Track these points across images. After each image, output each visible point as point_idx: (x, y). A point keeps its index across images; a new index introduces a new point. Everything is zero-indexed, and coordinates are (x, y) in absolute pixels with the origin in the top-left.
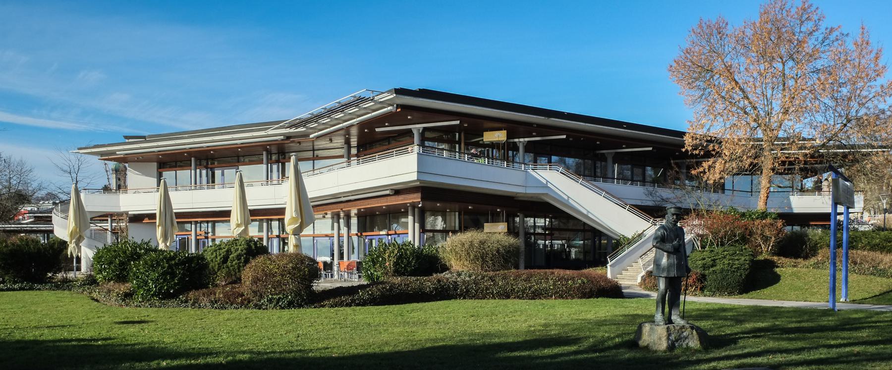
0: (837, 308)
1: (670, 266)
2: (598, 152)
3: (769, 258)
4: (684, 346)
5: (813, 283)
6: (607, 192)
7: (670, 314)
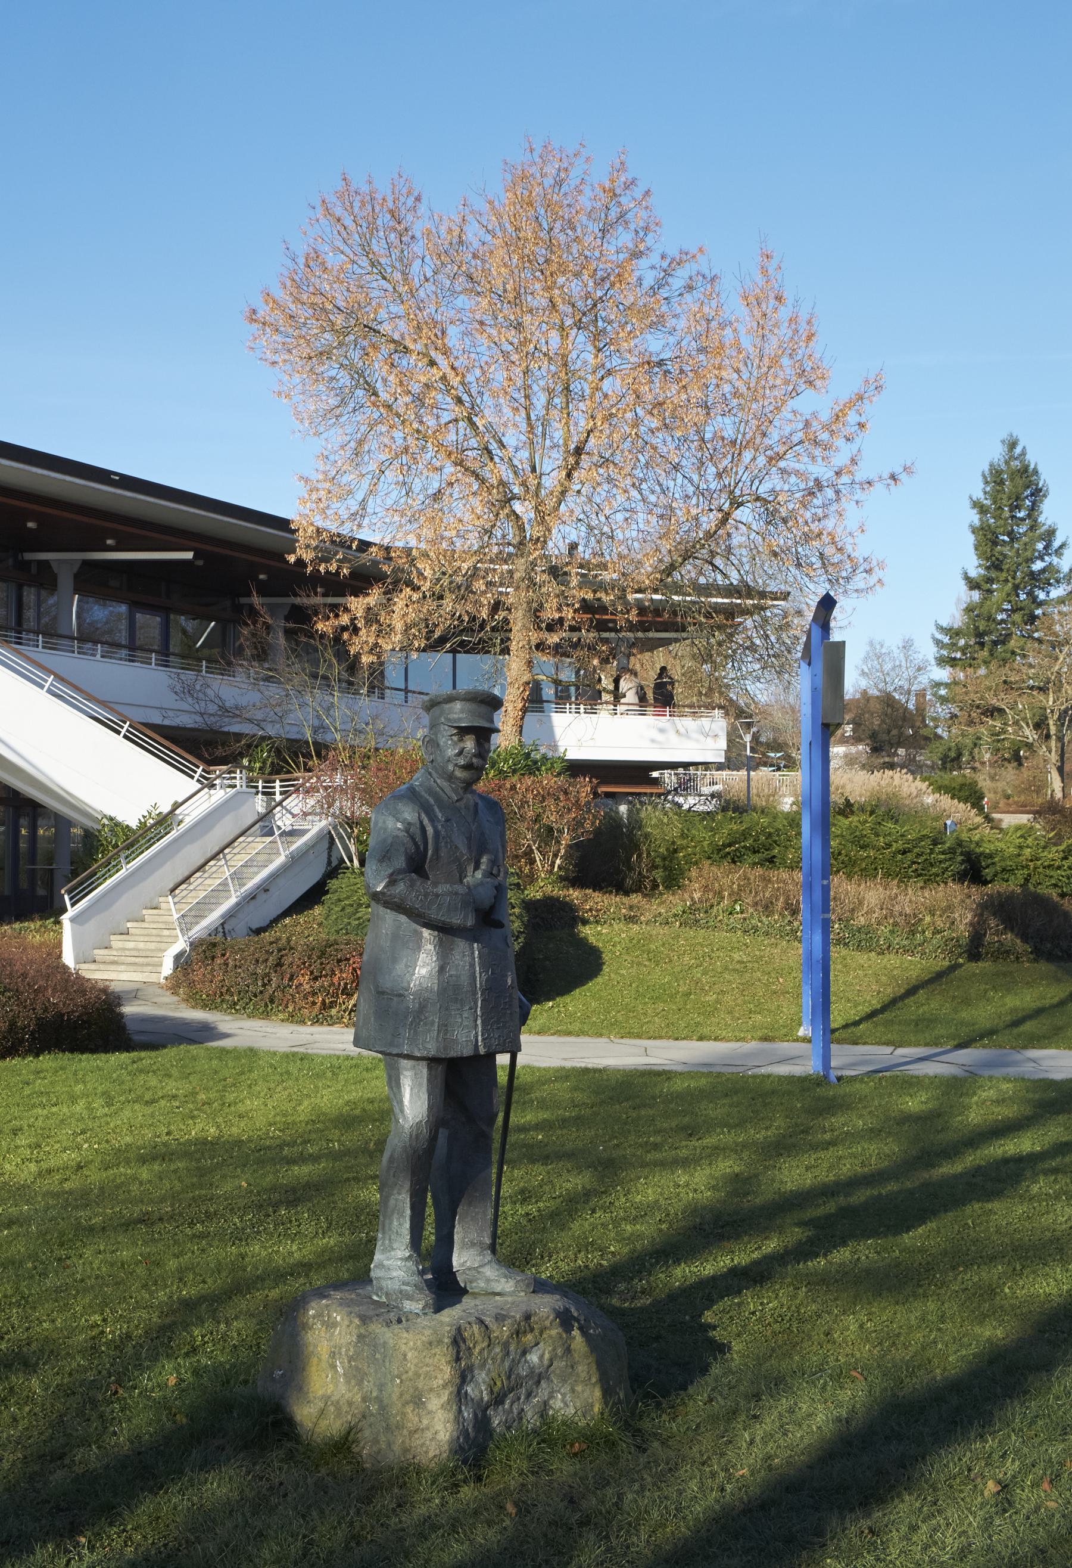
0: (833, 1074)
1: (449, 992)
2: (29, 556)
3: (558, 892)
4: (531, 1419)
5: (697, 973)
6: (59, 678)
7: (446, 1242)
